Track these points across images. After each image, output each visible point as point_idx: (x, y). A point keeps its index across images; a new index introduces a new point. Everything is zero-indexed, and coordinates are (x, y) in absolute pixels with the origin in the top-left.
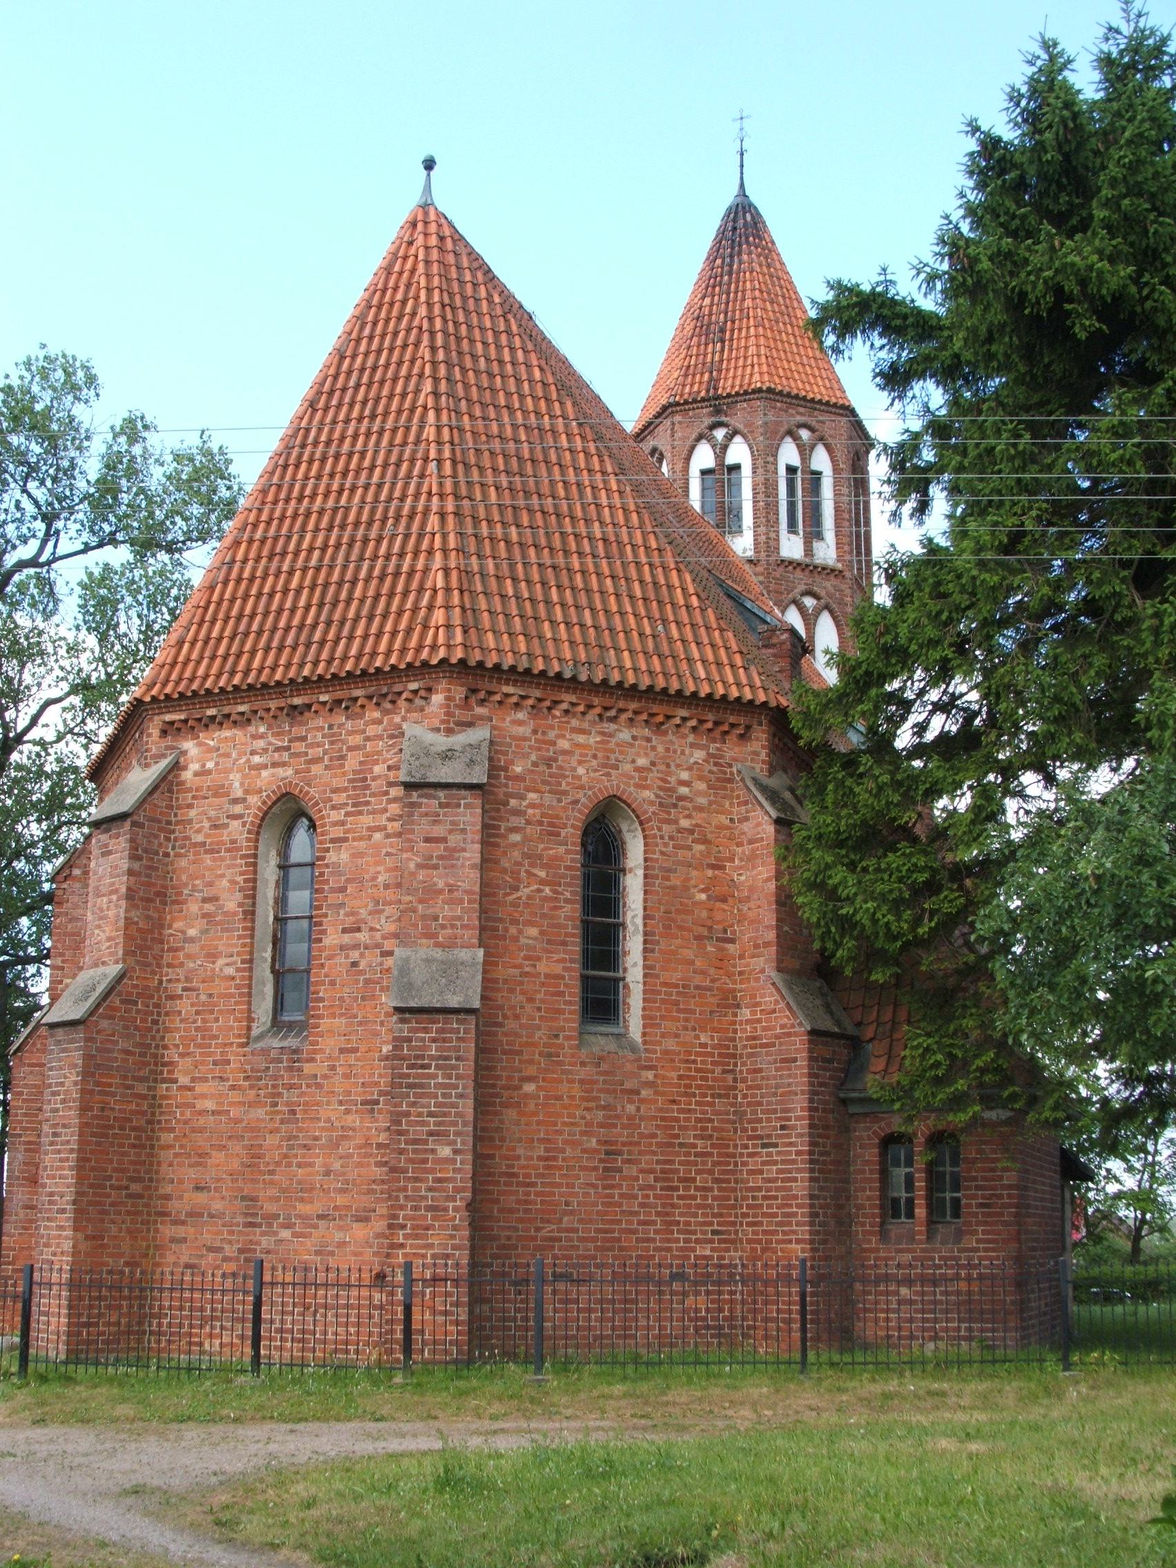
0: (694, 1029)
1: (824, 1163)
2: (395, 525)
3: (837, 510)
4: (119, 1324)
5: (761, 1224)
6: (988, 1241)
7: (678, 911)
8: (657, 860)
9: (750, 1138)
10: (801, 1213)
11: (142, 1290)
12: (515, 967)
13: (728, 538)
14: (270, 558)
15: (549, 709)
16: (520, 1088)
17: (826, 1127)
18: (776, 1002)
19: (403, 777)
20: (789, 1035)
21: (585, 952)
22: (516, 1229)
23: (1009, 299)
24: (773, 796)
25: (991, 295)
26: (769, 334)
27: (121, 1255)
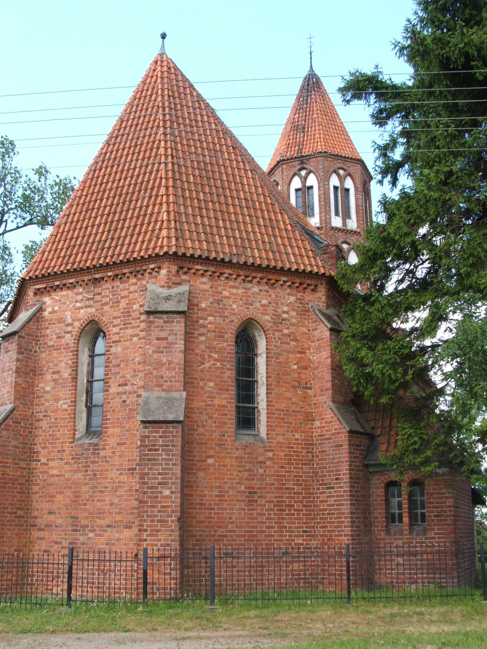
0: (292, 432)
1: (358, 496)
2: (145, 193)
3: (357, 205)
4: (12, 580)
5: (327, 527)
6: (441, 534)
7: (283, 374)
8: (272, 349)
9: (320, 485)
10: (347, 521)
11: (23, 563)
12: (203, 401)
13: (308, 218)
14: (87, 211)
15: (219, 277)
16: (206, 461)
17: (358, 478)
18: (332, 417)
19: (146, 308)
20: (339, 433)
21: (238, 395)
22: (205, 531)
23: (441, 62)
24: (329, 318)
25: (432, 57)
26: (325, 129)
27: (13, 546)
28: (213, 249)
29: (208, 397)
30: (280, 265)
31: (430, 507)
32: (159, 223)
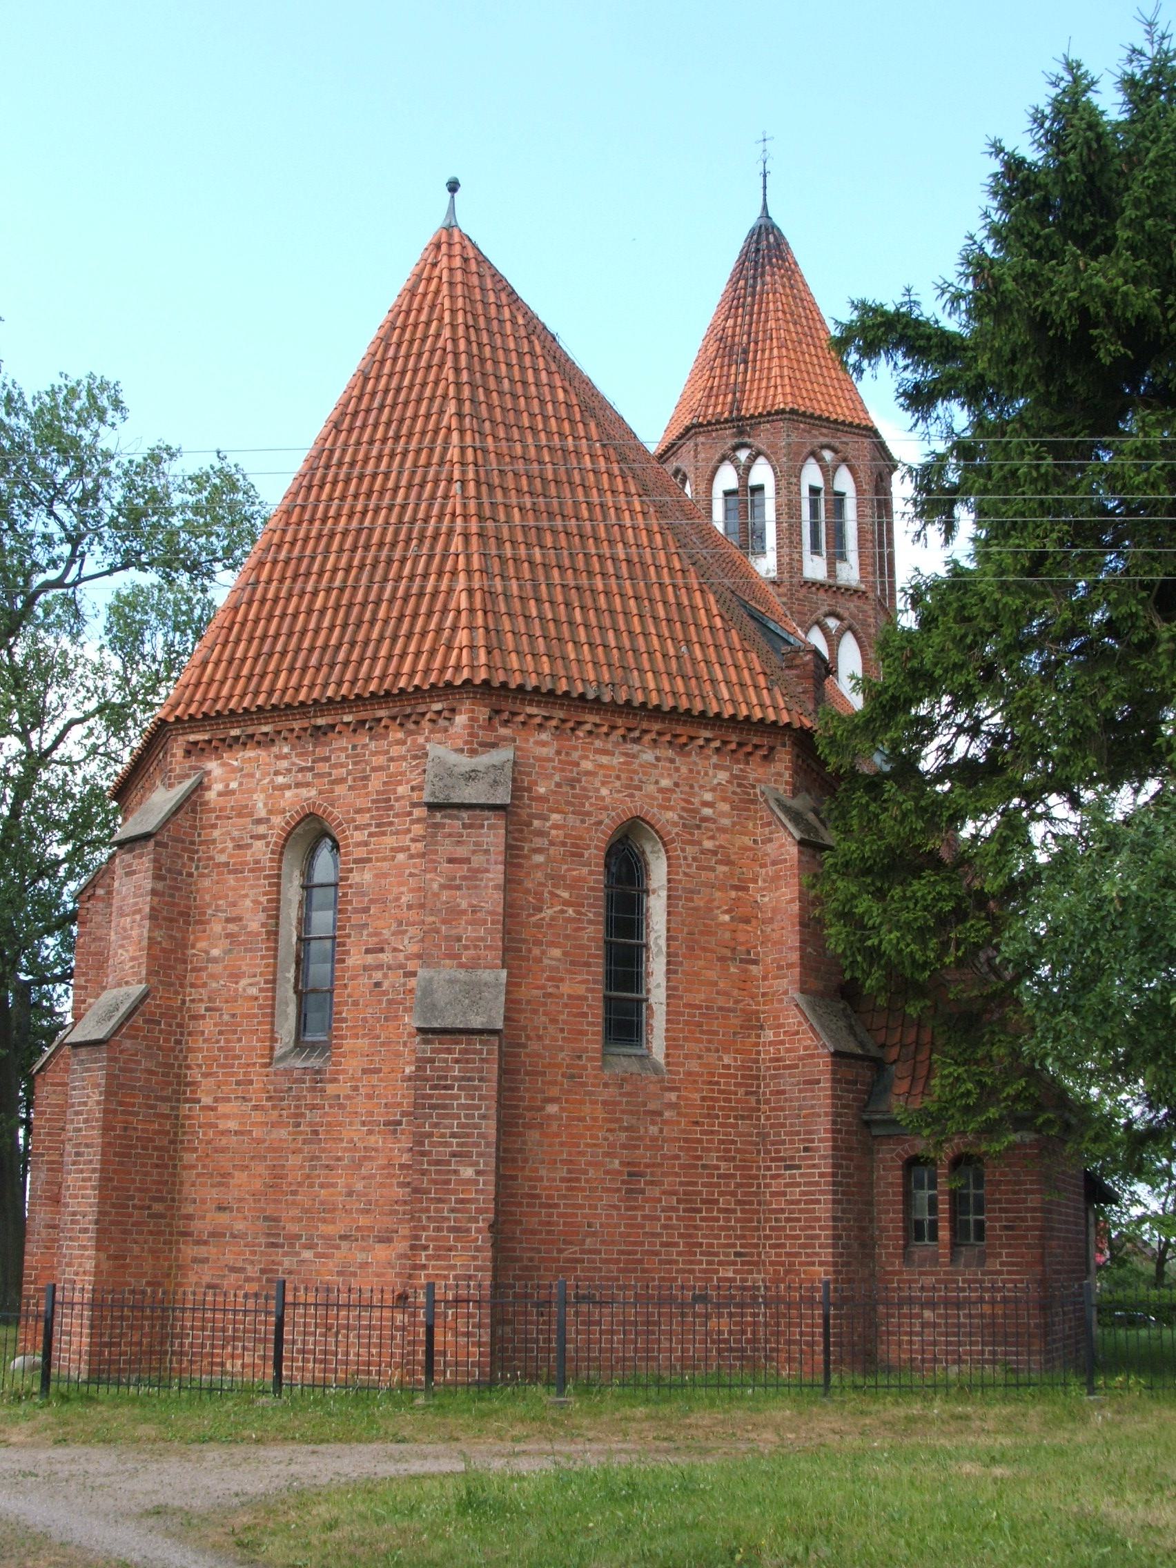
0: (717, 1051)
1: (848, 1185)
3: (860, 531)
5: (783, 1246)
6: (1013, 1264)
7: (702, 933)
9: (772, 1160)
10: (825, 1235)
11: (164, 1310)
12: (538, 988)
13: (751, 559)
14: (294, 579)
15: (573, 730)
16: (543, 1109)
17: (849, 1149)
18: (800, 1024)
19: (426, 798)
20: (812, 1056)
22: (539, 1251)
23: (1031, 320)
25: (1016, 315)
27: (144, 1275)
28: (562, 673)
29: (549, 979)
30: (698, 706)
31: (993, 1210)
32: (451, 615)
